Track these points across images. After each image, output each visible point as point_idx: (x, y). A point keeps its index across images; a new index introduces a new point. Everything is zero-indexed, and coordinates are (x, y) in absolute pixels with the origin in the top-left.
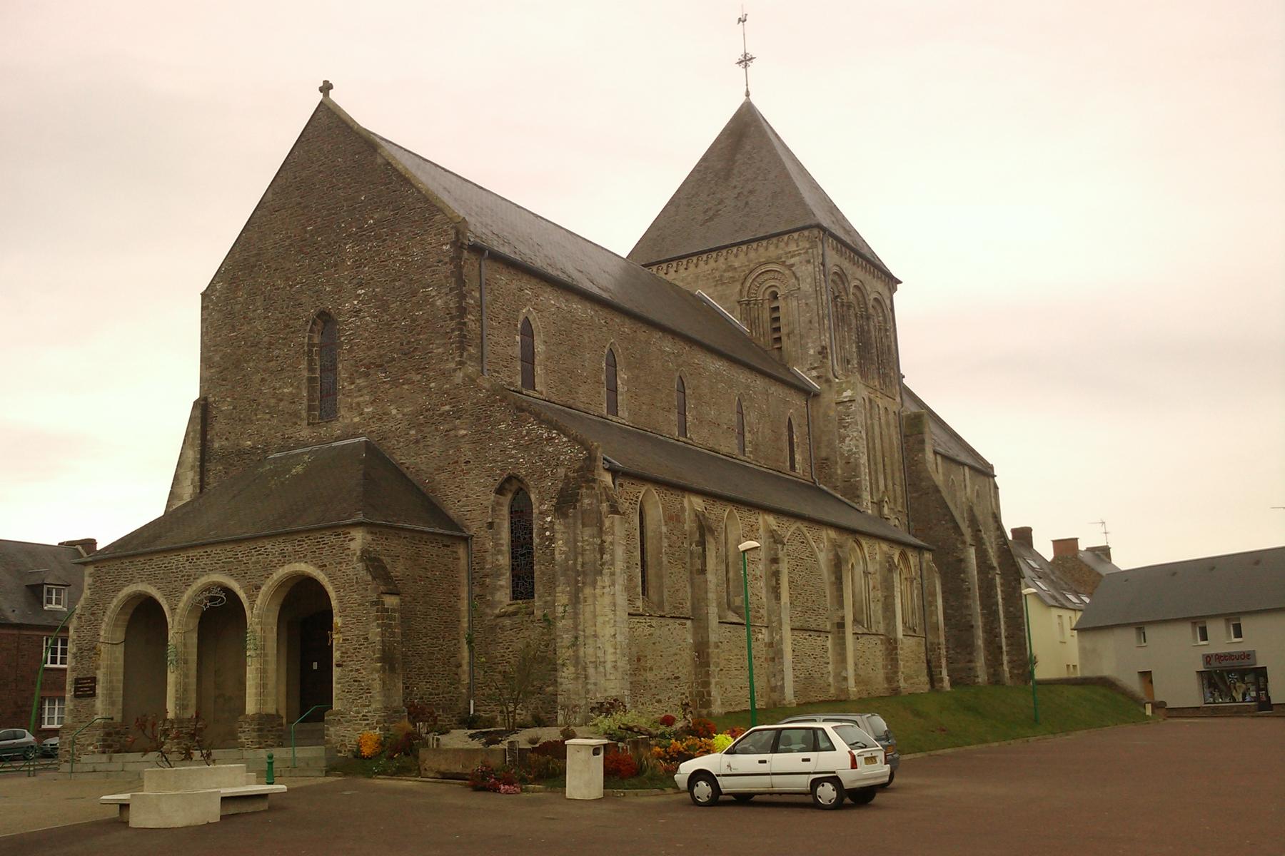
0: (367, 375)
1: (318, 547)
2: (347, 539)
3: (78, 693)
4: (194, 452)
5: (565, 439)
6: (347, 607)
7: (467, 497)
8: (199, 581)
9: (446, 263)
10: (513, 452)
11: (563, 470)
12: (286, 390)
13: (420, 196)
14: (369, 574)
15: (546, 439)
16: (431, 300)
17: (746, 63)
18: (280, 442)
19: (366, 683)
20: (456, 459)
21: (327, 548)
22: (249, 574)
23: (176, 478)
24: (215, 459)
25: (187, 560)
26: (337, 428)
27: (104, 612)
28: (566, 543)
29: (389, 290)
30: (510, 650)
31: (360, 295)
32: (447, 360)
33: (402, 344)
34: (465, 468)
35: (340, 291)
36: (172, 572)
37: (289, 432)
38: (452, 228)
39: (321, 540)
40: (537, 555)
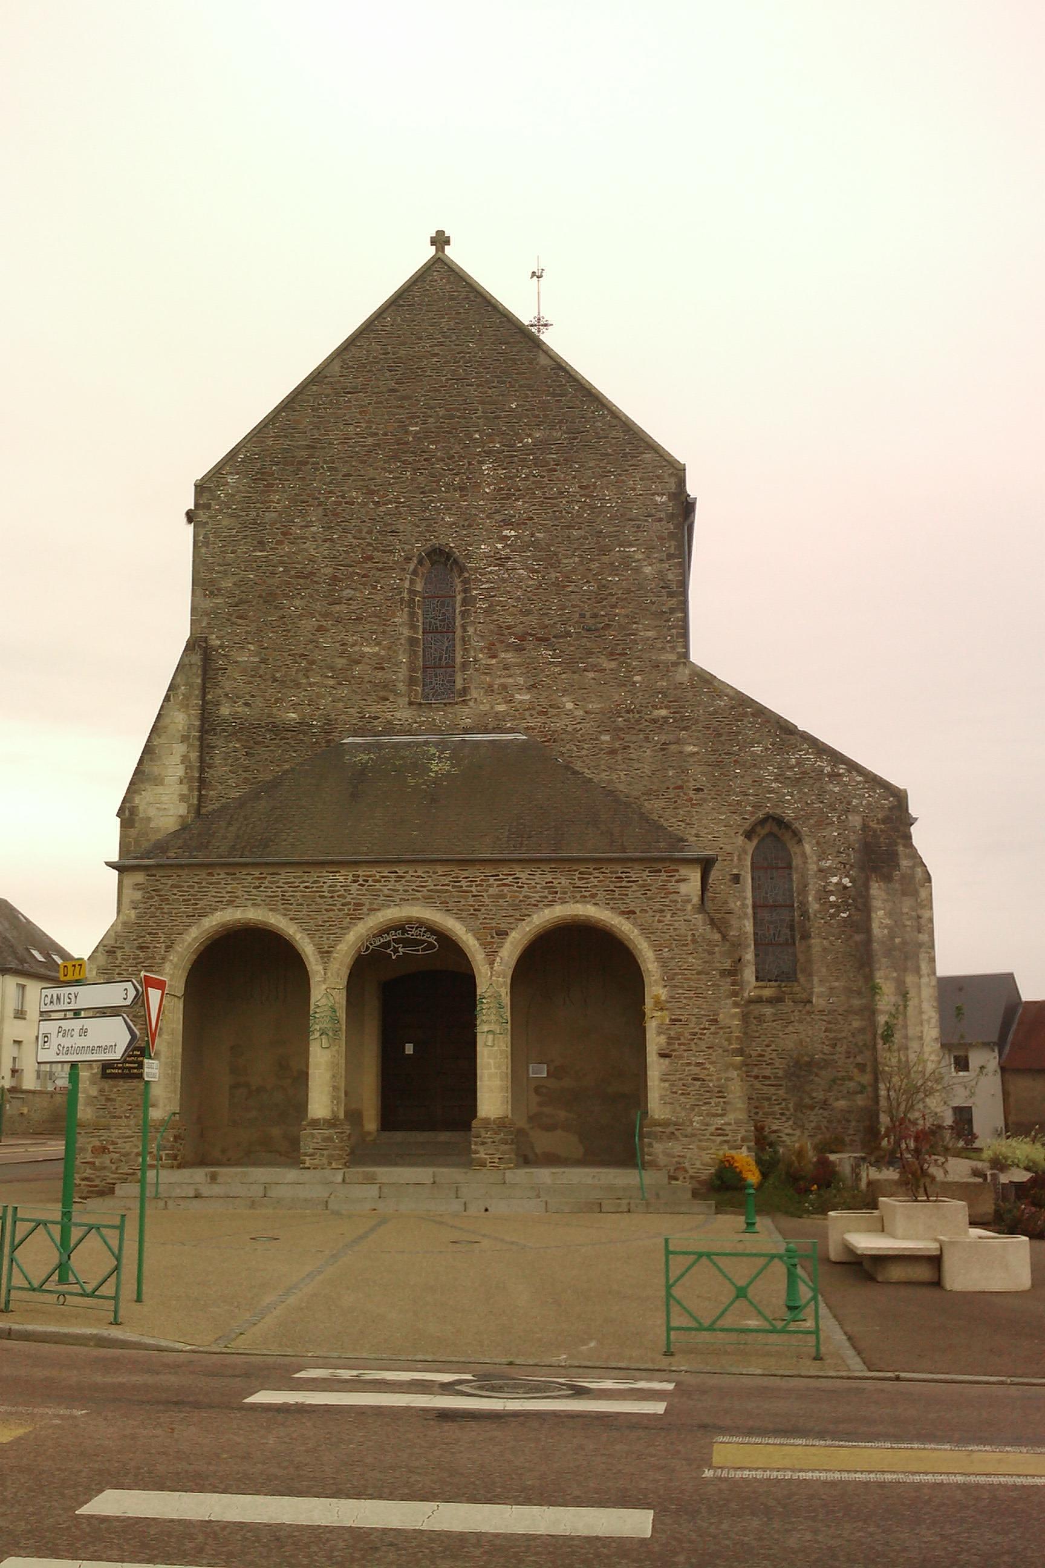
0: (520, 649)
1: (618, 885)
2: (673, 879)
3: (108, 1071)
4: (189, 715)
5: (859, 779)
6: (676, 974)
7: (697, 835)
8: (379, 914)
9: (660, 520)
10: (773, 785)
11: (857, 818)
12: (366, 649)
13: (615, 422)
14: (715, 931)
15: (829, 775)
16: (634, 564)
17: (539, 322)
18: (354, 722)
19: (716, 1084)
20: (680, 783)
21: (635, 888)
22: (483, 911)
23: (148, 751)
24: (224, 730)
25: (355, 881)
26: (465, 715)
27: (168, 947)
28: (890, 914)
29: (560, 540)
30: (773, 1047)
31: (507, 537)
32: (663, 648)
33: (582, 616)
34: (694, 797)
35: (470, 526)
36: (321, 897)
37: (373, 709)
38: (671, 475)
39: (624, 875)
40: (817, 925)
